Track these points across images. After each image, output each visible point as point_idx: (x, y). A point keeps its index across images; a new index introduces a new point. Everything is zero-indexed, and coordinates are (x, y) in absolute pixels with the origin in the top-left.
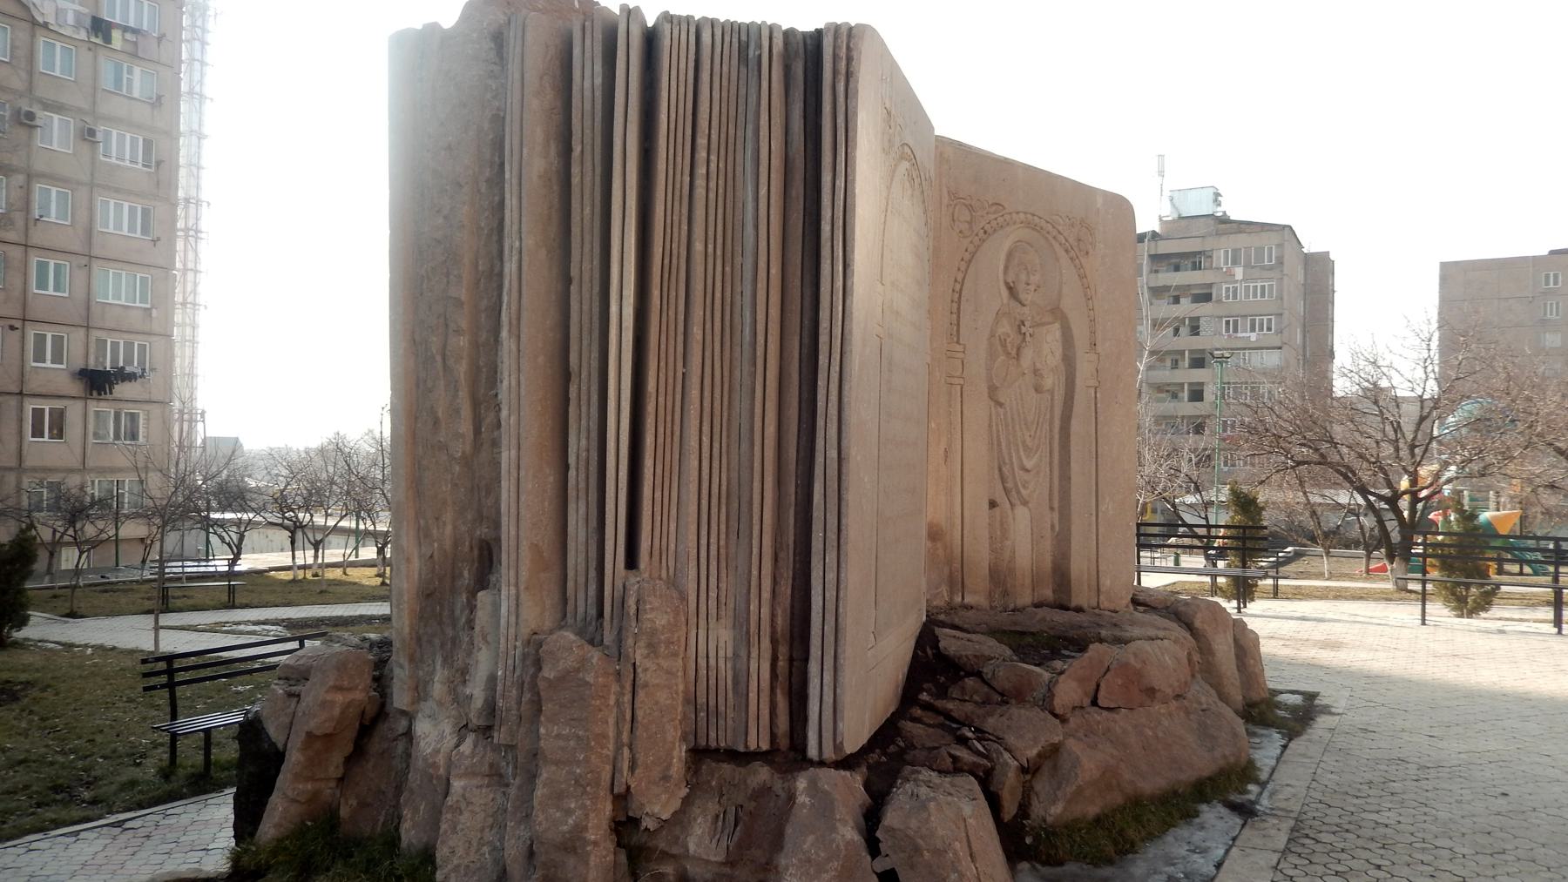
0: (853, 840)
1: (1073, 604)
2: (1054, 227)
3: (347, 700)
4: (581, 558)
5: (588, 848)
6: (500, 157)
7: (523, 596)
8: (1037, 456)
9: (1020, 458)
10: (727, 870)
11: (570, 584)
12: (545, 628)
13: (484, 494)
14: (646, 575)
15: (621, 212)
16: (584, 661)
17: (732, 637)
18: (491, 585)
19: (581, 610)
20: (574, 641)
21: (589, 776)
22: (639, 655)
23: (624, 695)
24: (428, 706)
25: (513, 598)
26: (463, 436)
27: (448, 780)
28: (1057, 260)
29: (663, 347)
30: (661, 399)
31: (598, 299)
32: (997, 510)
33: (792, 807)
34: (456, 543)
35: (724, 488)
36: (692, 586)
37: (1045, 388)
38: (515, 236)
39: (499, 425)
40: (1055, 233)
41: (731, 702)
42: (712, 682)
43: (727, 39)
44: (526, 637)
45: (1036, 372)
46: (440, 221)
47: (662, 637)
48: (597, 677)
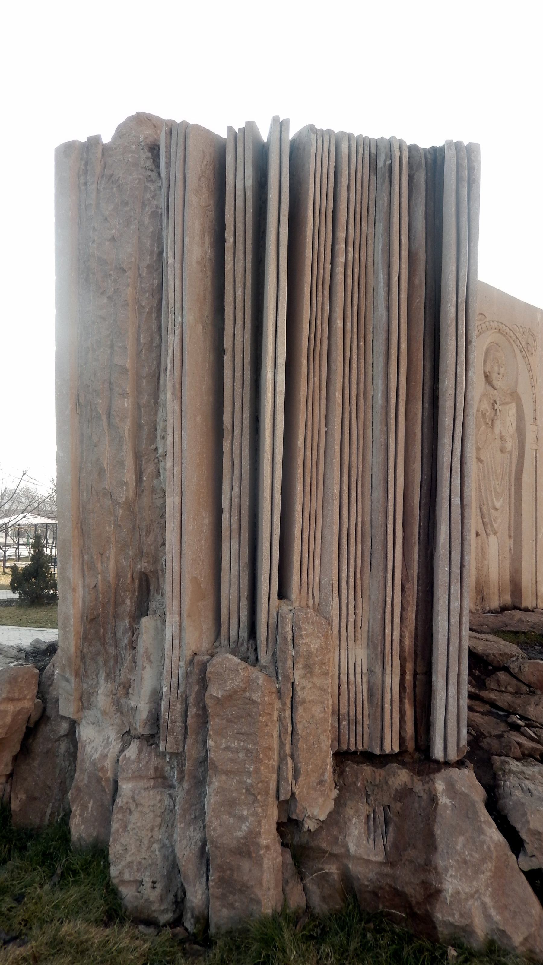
0: (499, 841)
1: (523, 605)
2: (513, 333)
3: (18, 709)
4: (234, 588)
5: (262, 852)
6: (158, 247)
7: (186, 623)
8: (502, 498)
9: (492, 500)
10: (387, 870)
11: (224, 611)
12: (203, 649)
13: (144, 533)
14: (296, 604)
15: (276, 292)
16: (249, 683)
17: (366, 656)
18: (150, 612)
19: (234, 633)
20: (239, 664)
21: (259, 785)
22: (298, 675)
23: (284, 710)
24: (91, 714)
25: (177, 625)
26: (126, 484)
27: (116, 783)
28: (515, 357)
29: (310, 408)
30: (308, 453)
31: (249, 367)
32: (479, 538)
33: (436, 808)
34: (118, 575)
35: (359, 529)
36: (336, 613)
37: (508, 450)
38: (178, 312)
39: (158, 474)
40: (514, 337)
41: (366, 713)
42: (352, 694)
43: (361, 151)
44: (188, 658)
45: (502, 438)
46: (105, 300)
47: (317, 659)
48: (264, 696)
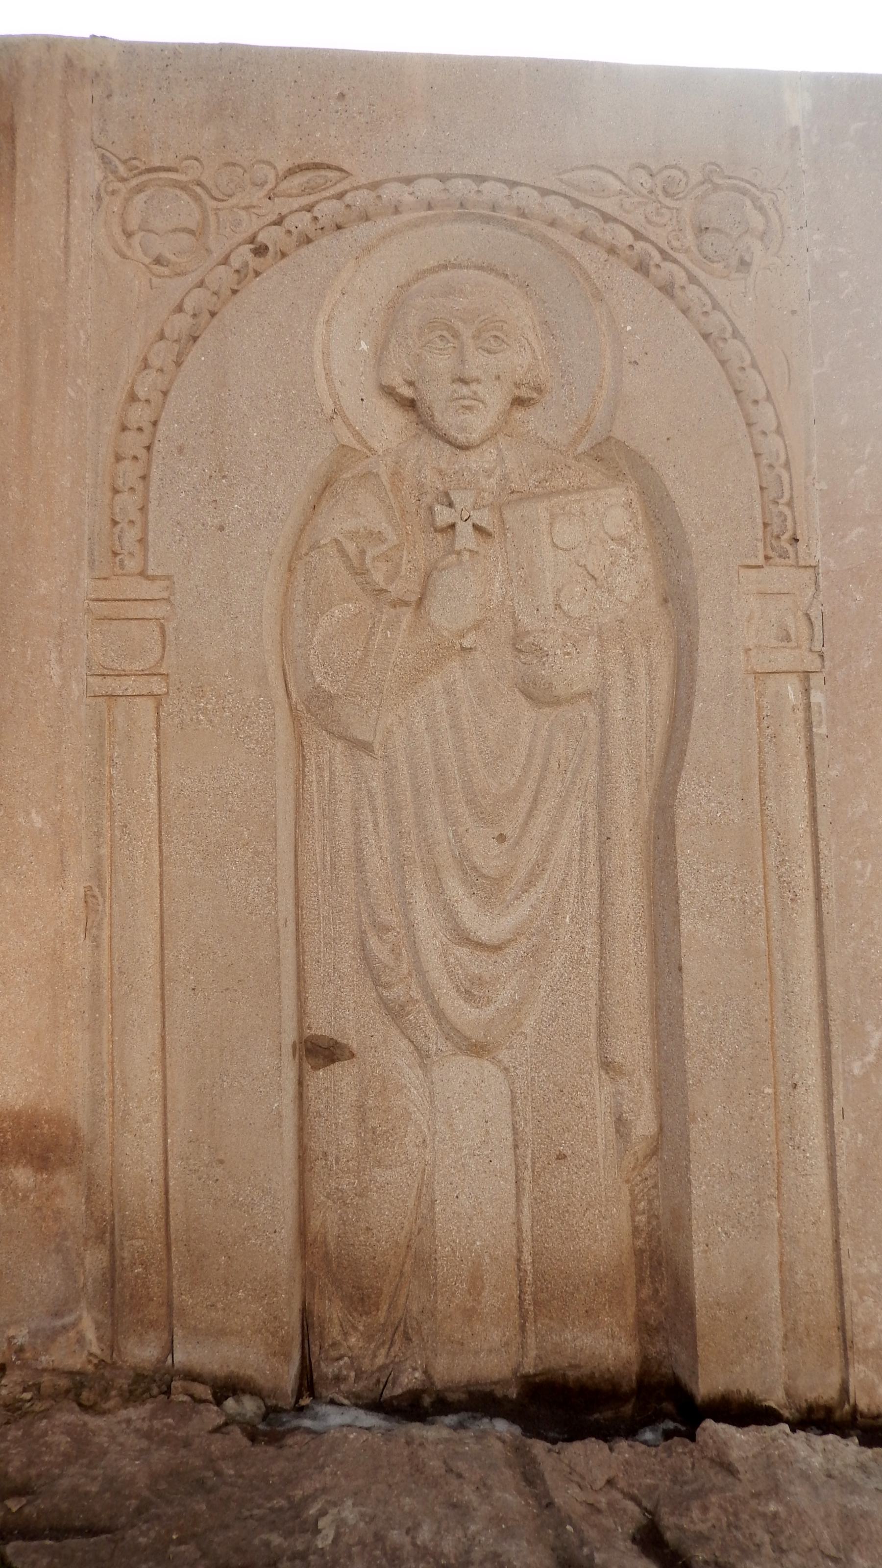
2: (577, 204)
